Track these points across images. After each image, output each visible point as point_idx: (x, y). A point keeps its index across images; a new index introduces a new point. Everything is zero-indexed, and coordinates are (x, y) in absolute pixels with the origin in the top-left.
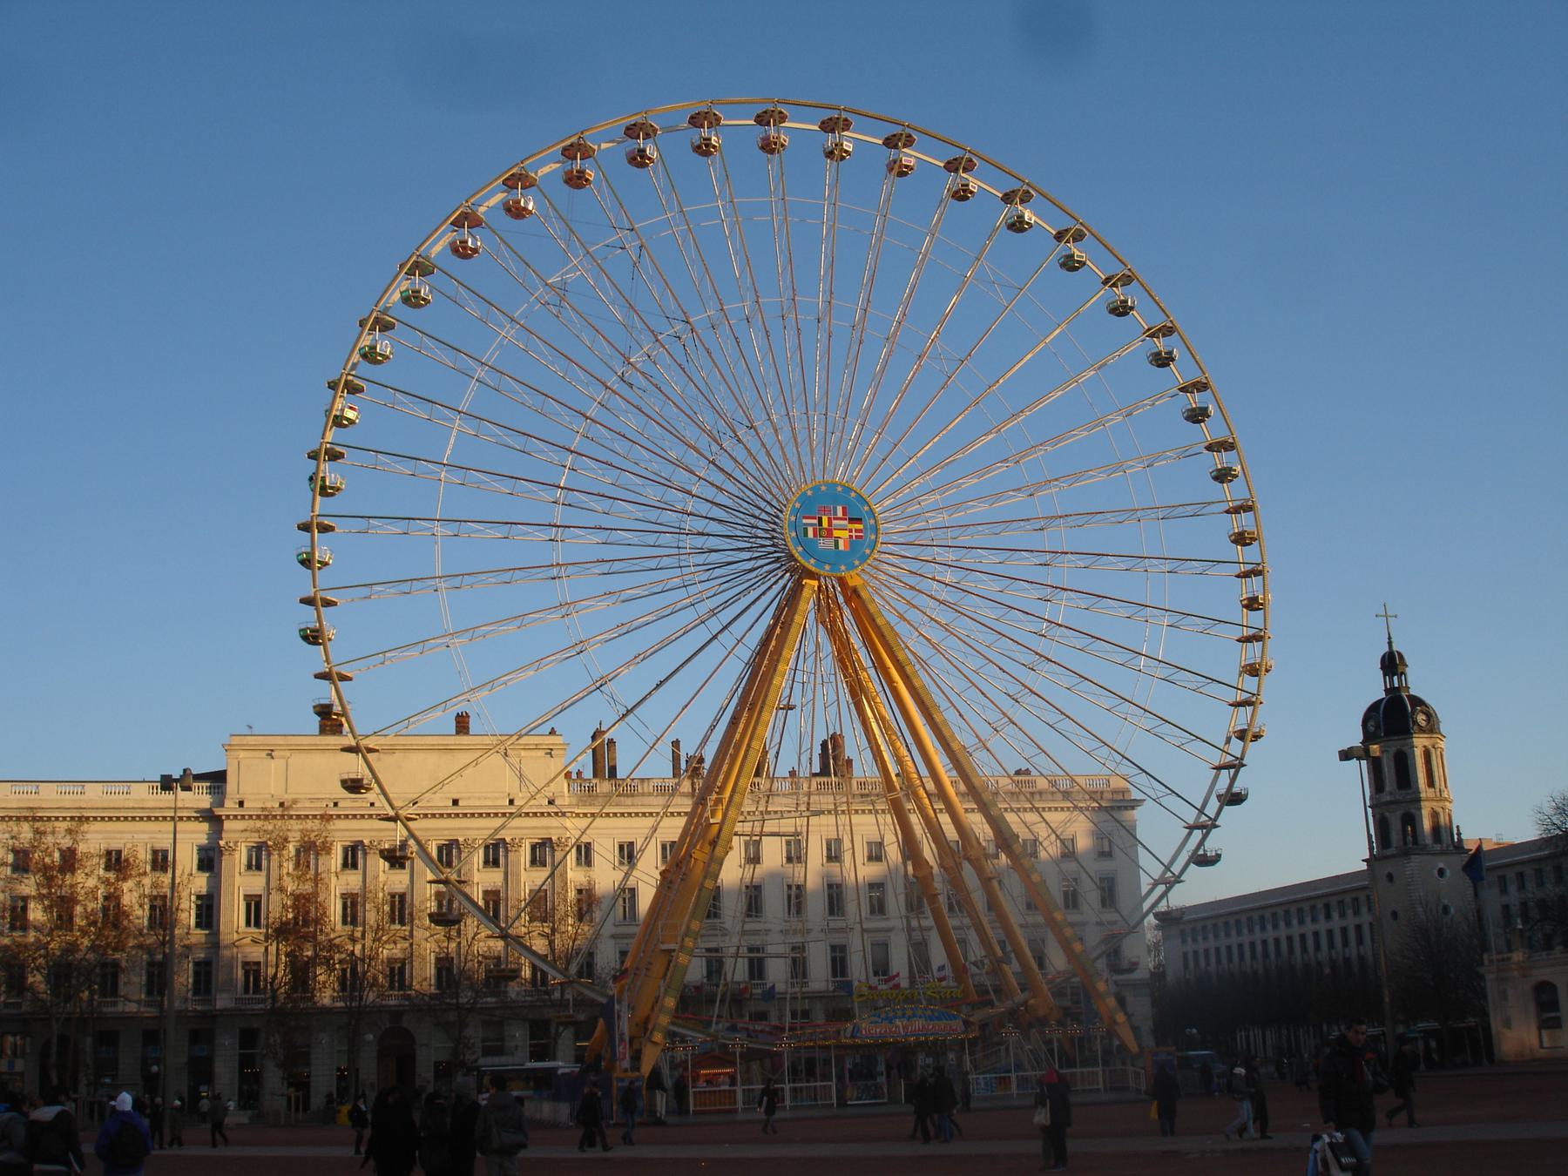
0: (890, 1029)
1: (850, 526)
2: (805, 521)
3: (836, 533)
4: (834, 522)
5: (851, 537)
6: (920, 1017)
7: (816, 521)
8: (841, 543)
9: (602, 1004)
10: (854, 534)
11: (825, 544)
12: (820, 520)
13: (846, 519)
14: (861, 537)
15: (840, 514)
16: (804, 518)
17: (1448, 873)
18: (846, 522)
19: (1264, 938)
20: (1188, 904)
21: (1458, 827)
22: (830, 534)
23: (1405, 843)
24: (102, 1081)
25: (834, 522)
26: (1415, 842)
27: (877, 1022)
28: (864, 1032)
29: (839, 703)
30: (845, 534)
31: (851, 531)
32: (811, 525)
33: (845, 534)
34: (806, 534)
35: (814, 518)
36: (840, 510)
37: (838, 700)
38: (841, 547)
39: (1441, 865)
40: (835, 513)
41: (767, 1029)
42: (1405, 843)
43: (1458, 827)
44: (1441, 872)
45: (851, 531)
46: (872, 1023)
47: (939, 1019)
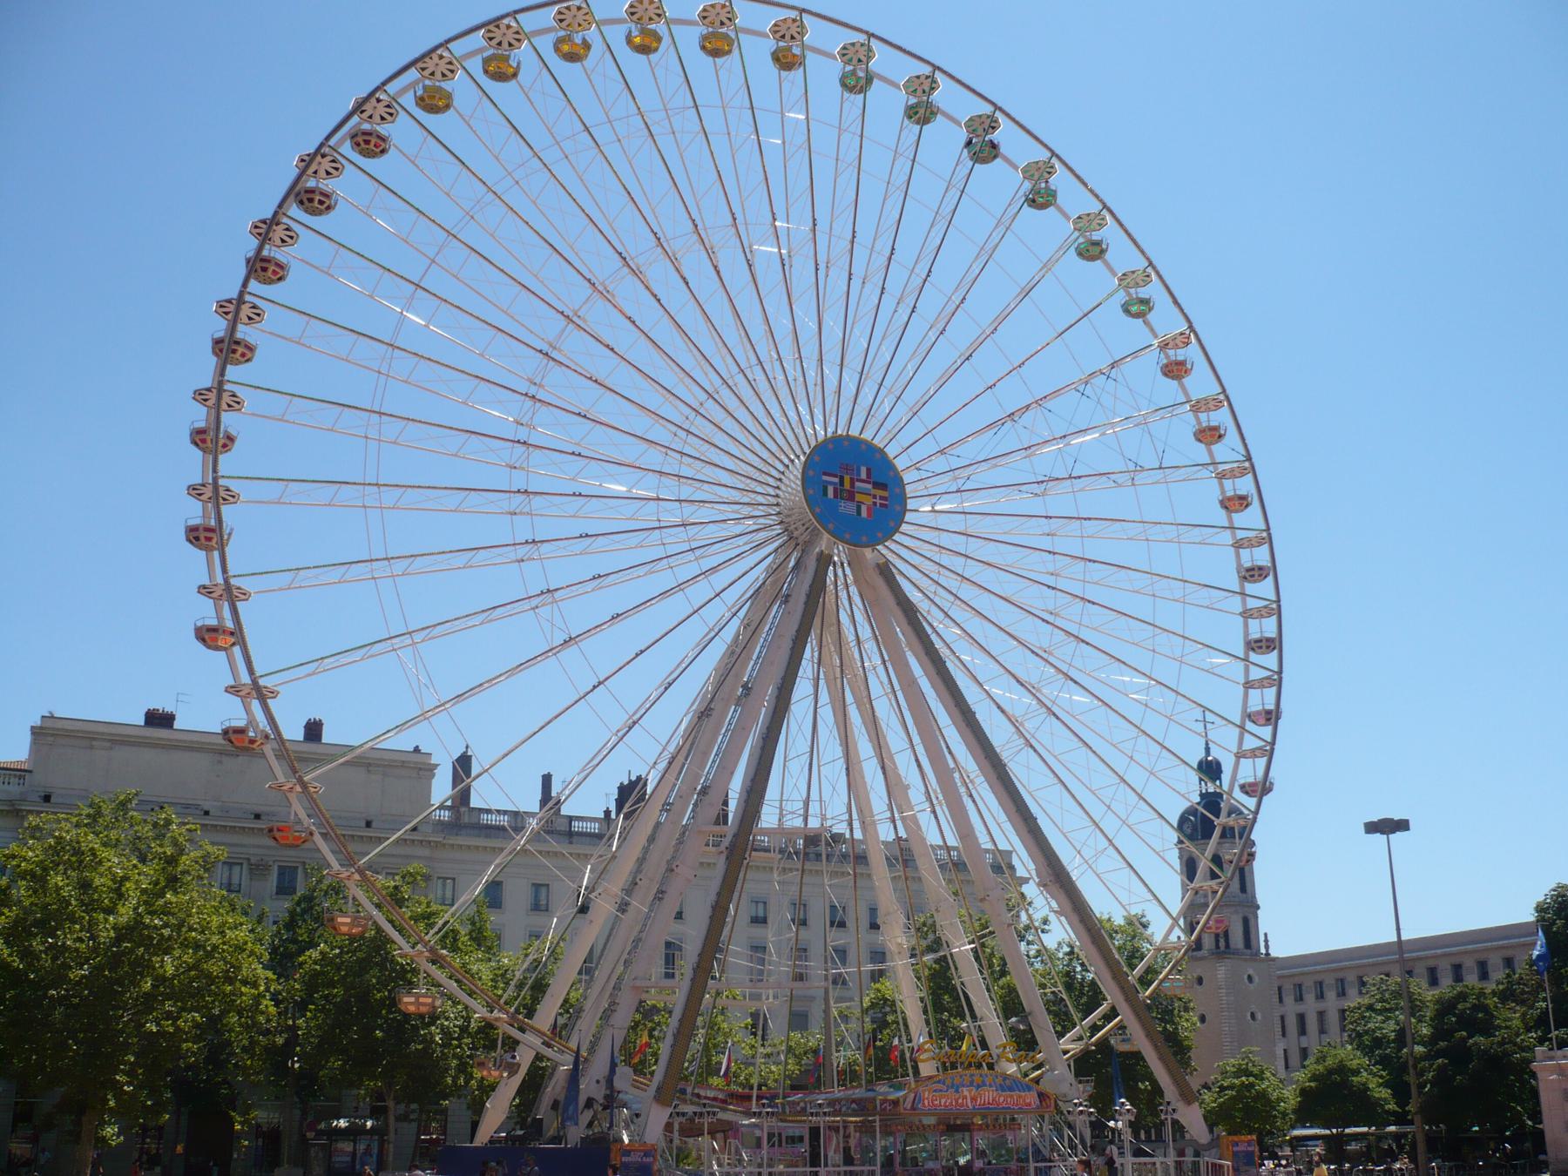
0: (957, 1101)
1: (874, 491)
2: (825, 478)
3: (858, 497)
4: (858, 484)
5: (875, 504)
6: (990, 1086)
7: (836, 480)
8: (864, 509)
9: (1066, 918)
10: (878, 501)
11: (847, 508)
12: (842, 479)
13: (869, 483)
14: (885, 506)
15: (864, 476)
16: (825, 474)
17: (1256, 979)
18: (869, 486)
19: (1300, 1011)
20: (1281, 956)
21: (1266, 935)
22: (851, 496)
23: (1217, 946)
24: (710, 1081)
25: (858, 484)
26: (1227, 946)
27: (941, 1091)
28: (926, 1102)
29: (785, 758)
30: (869, 501)
31: (875, 497)
32: (831, 483)
33: (869, 501)
34: (825, 493)
35: (835, 476)
36: (863, 470)
37: (785, 761)
38: (864, 513)
39: (1251, 972)
40: (859, 473)
41: (721, 1096)
42: (1217, 946)
43: (1266, 935)
44: (1250, 978)
45: (875, 497)
46: (935, 1091)
47: (1011, 1089)
